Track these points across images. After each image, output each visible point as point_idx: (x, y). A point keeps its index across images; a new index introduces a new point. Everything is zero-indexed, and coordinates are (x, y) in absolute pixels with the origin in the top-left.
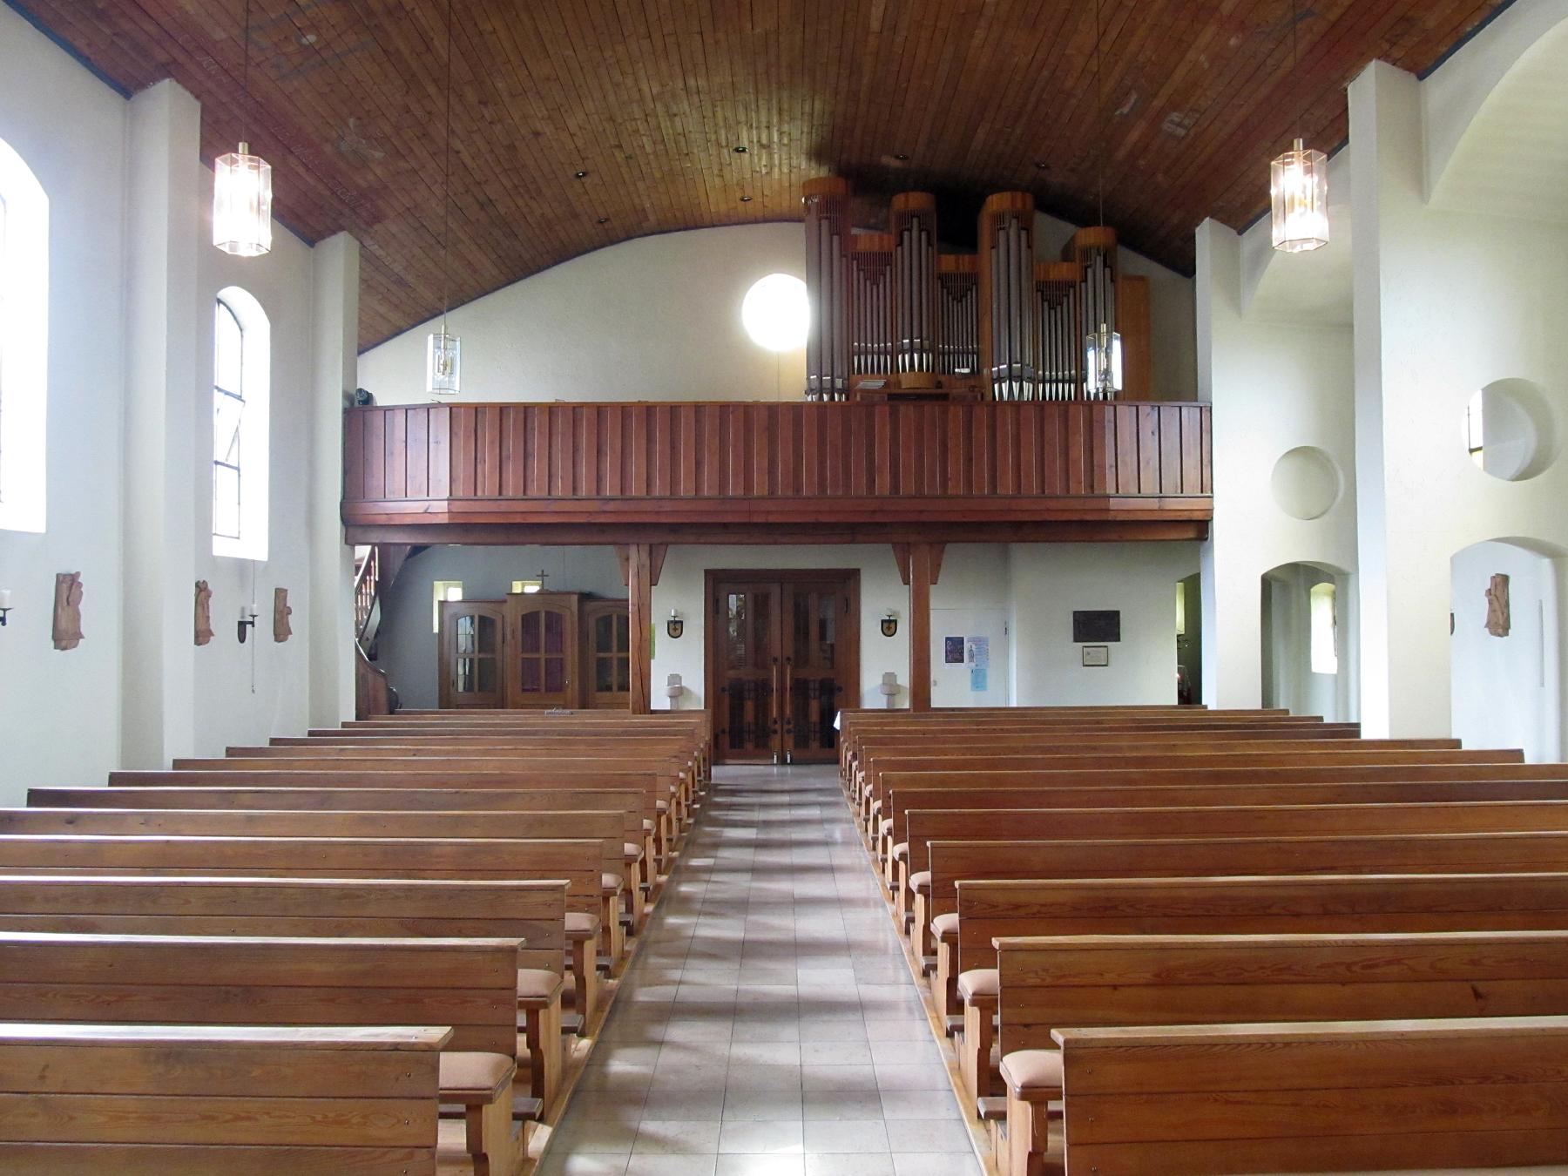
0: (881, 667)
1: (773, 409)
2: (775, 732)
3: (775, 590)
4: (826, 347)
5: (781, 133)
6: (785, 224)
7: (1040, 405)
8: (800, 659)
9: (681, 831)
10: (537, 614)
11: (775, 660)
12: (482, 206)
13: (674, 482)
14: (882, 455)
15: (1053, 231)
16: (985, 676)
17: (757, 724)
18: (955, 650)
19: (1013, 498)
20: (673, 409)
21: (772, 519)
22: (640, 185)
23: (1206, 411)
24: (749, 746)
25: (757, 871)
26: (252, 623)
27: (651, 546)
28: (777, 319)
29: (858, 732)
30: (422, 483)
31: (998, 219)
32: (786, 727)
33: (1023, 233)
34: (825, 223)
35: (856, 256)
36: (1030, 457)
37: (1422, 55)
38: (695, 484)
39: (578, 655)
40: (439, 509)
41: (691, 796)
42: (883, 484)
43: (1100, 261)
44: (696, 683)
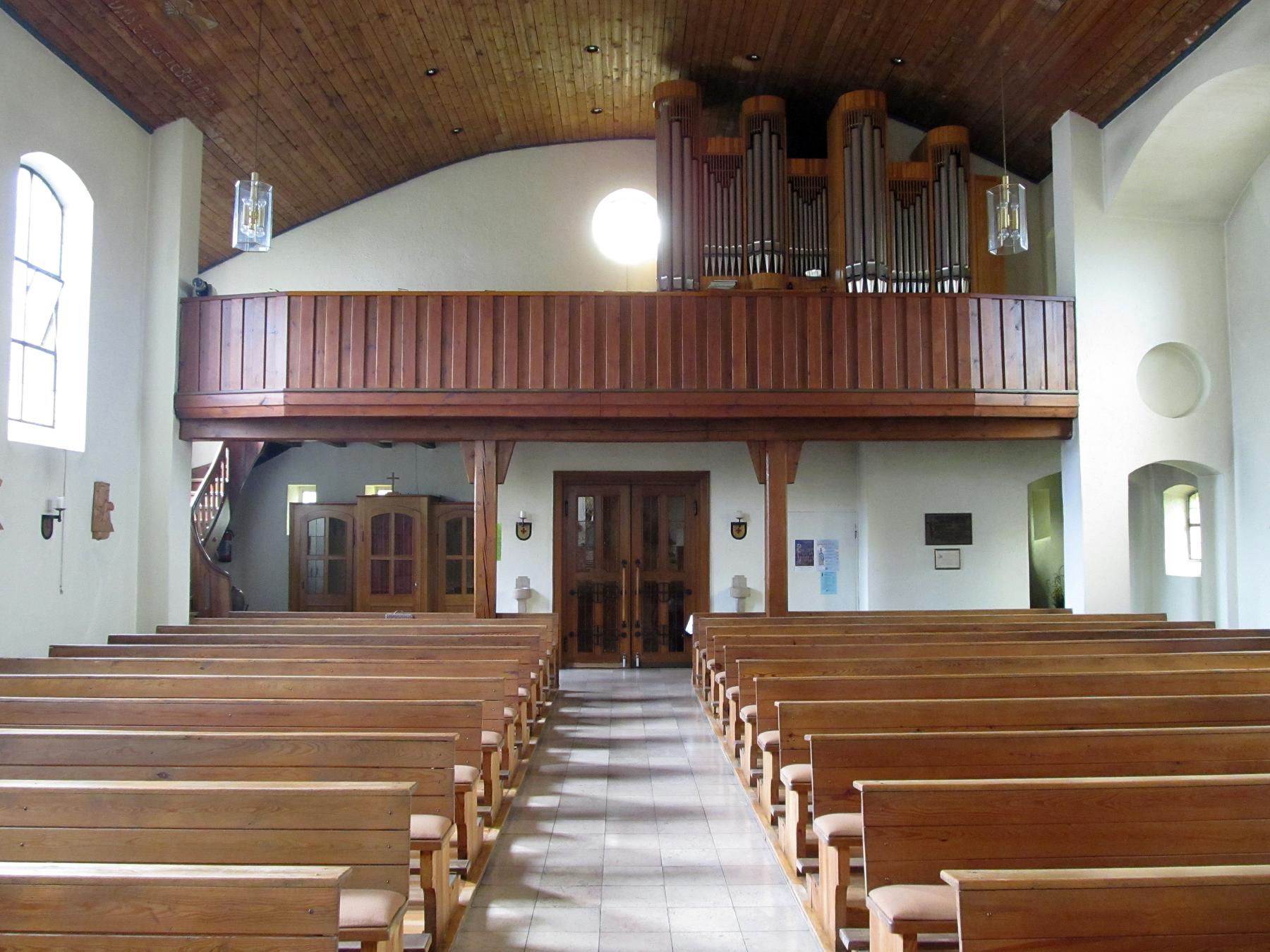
0: (733, 571)
1: (625, 300)
2: (624, 635)
3: (624, 493)
4: (677, 255)
5: (633, 28)
6: (634, 141)
7: (903, 298)
8: (648, 564)
9: (521, 756)
10: (388, 515)
11: (624, 562)
12: (331, 100)
13: (521, 375)
14: (738, 348)
15: (903, 136)
16: (834, 581)
17: (604, 626)
18: (806, 554)
19: (873, 393)
20: (521, 299)
21: (625, 413)
22: (492, 89)
23: (1069, 305)
24: (598, 650)
25: (610, 774)
26: (59, 517)
27: (497, 442)
28: (627, 232)
29: (722, 641)
30: (261, 374)
31: (851, 118)
32: (635, 630)
33: (876, 132)
34: (676, 126)
35: (706, 160)
36: (892, 348)
37: (1102, 109)
38: (543, 378)
39: (427, 558)
40: (274, 401)
41: (535, 710)
42: (740, 377)
43: (953, 159)
44: (544, 586)
